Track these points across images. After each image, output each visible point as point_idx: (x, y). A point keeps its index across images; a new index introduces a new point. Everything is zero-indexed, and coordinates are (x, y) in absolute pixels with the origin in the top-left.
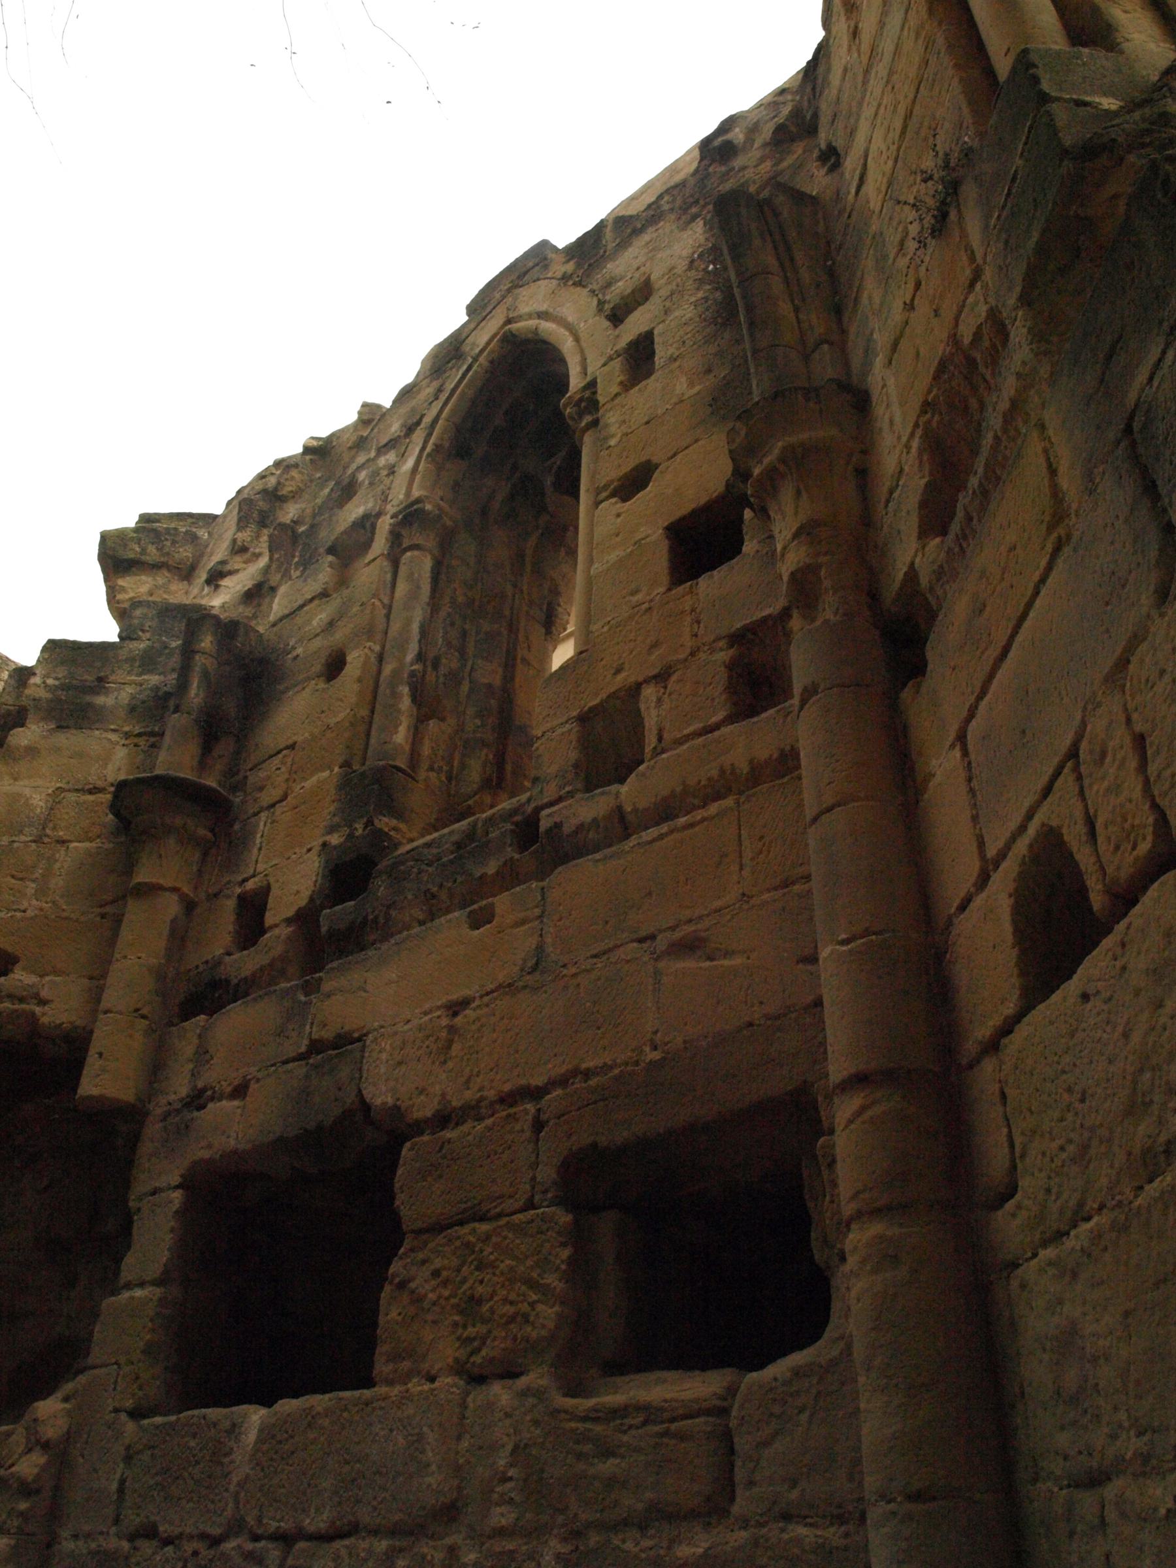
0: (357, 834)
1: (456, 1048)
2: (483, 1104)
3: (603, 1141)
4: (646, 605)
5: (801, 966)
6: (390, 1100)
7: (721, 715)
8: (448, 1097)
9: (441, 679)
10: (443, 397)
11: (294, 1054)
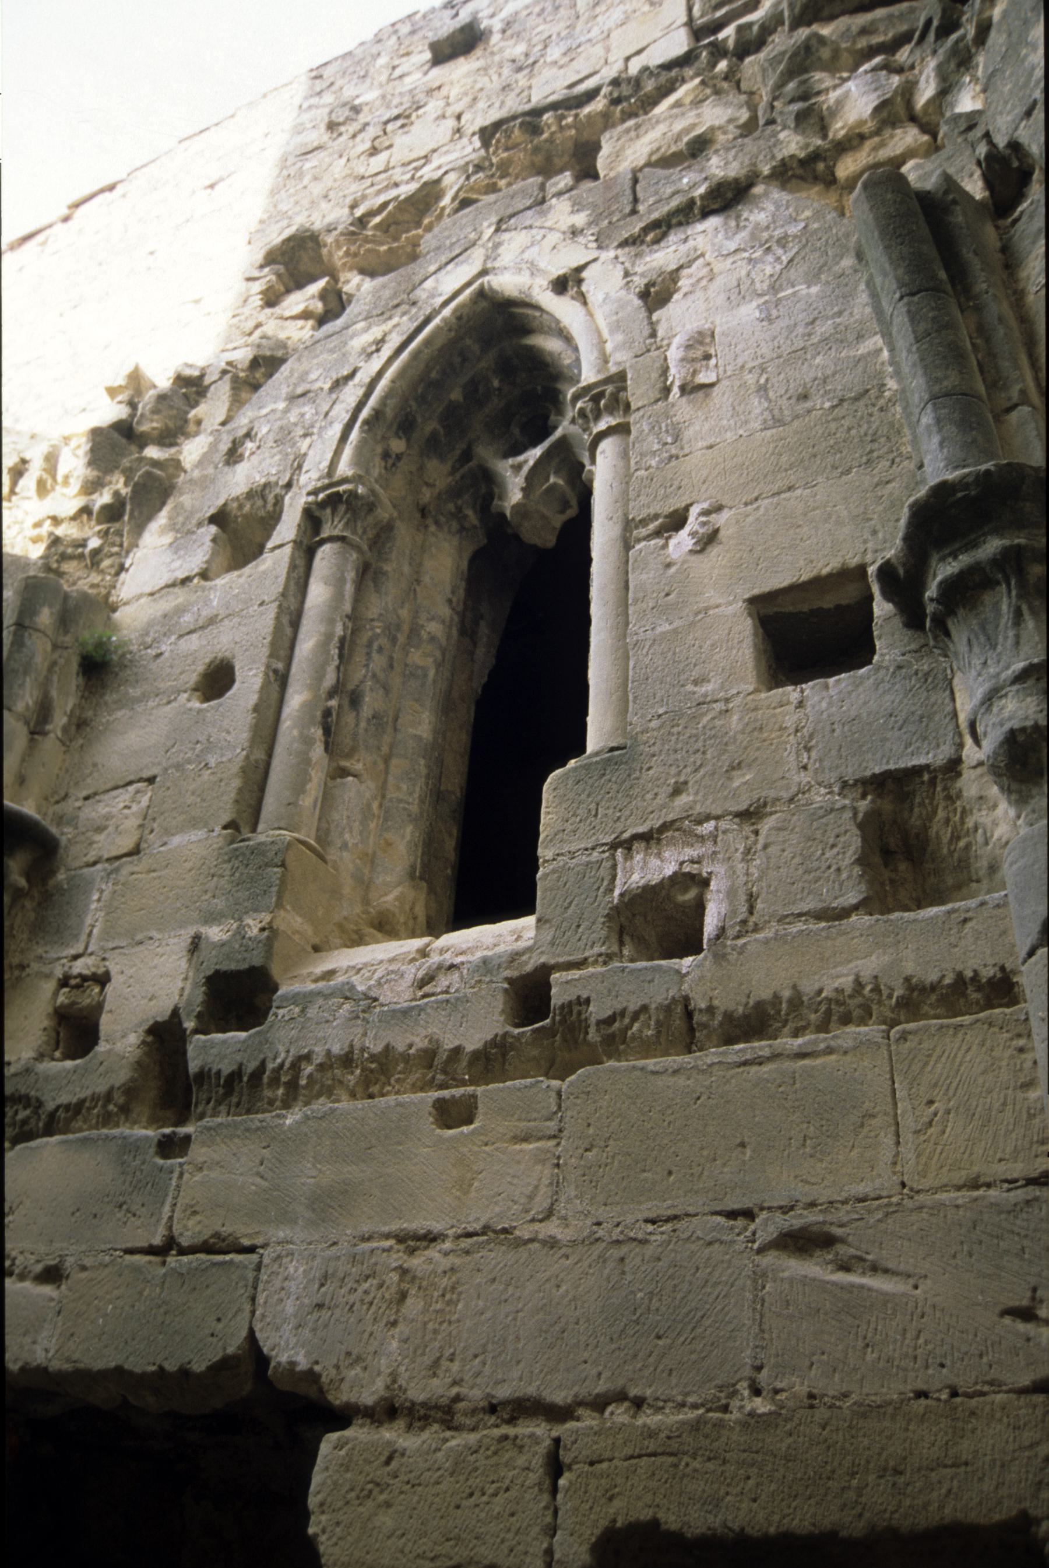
0: (249, 934)
1: (413, 1306)
2: (461, 1405)
3: (671, 1521)
4: (719, 706)
5: (1007, 1320)
6: (303, 1362)
7: (852, 898)
8: (401, 1381)
9: (363, 725)
10: (387, 351)
11: (146, 1245)
